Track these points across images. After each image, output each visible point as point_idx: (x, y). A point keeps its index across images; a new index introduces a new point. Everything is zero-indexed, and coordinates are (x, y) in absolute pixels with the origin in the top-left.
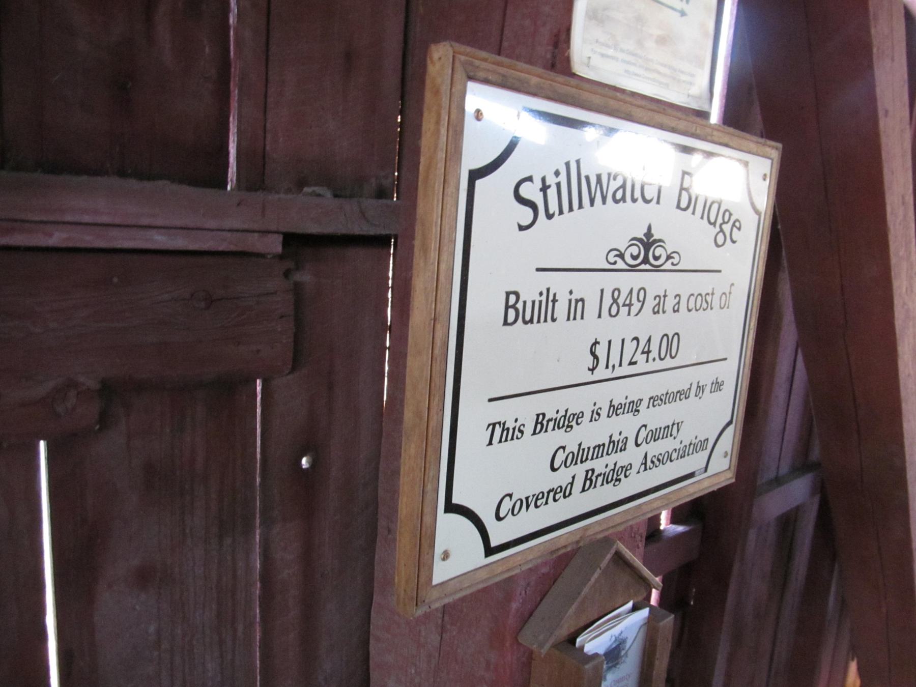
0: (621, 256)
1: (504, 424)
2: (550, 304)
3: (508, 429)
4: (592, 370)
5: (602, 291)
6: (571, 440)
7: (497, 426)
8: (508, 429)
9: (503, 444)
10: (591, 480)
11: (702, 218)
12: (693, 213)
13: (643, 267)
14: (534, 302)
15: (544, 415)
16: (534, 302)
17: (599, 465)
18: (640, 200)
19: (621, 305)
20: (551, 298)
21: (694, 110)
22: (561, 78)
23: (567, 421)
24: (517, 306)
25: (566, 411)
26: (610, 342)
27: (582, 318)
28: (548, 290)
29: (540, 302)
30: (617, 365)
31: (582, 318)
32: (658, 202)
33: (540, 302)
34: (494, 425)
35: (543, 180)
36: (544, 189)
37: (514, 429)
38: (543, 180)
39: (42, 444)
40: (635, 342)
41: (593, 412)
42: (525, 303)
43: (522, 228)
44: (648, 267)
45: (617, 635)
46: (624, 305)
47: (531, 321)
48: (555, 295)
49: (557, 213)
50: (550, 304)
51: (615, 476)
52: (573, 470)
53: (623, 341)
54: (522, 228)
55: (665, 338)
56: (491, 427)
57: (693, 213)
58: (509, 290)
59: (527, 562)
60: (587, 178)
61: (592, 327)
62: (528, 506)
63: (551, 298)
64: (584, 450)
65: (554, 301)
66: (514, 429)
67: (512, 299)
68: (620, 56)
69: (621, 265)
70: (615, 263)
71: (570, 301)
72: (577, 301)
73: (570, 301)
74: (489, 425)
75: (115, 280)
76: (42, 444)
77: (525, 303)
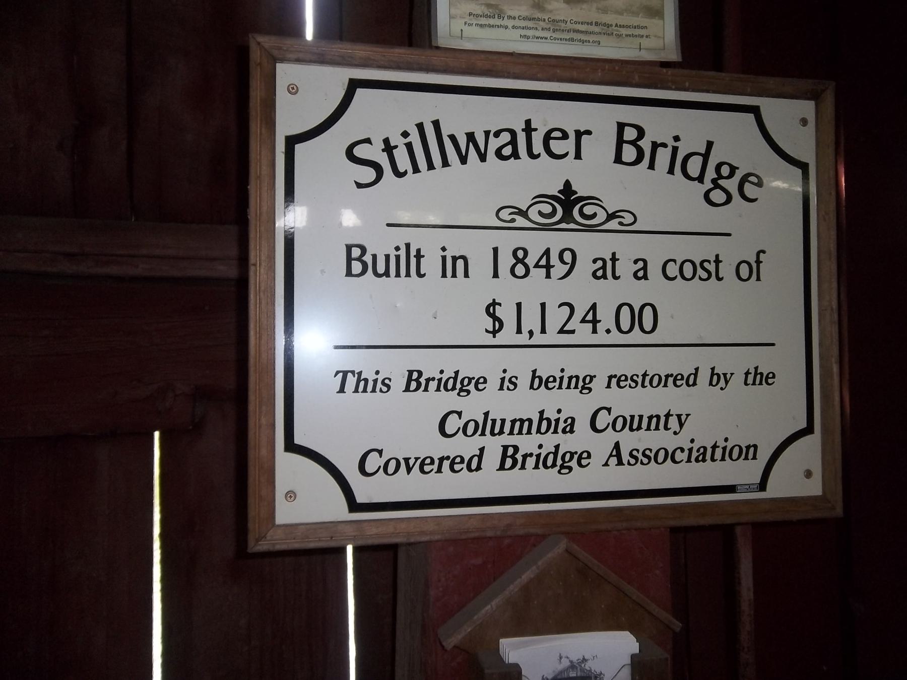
0: (524, 214)
1: (360, 373)
2: (413, 261)
3: (366, 380)
4: (494, 333)
5: (496, 250)
6: (473, 406)
7: (350, 375)
8: (366, 380)
9: (360, 395)
10: (513, 457)
11: (671, 171)
12: (651, 166)
13: (563, 226)
14: (387, 257)
15: (420, 373)
16: (387, 257)
17: (527, 443)
18: (544, 154)
19: (531, 266)
20: (413, 253)
21: (661, 62)
22: (429, 52)
23: (461, 385)
24: (364, 258)
25: (457, 373)
26: (519, 305)
27: (466, 275)
28: (408, 246)
29: (398, 258)
30: (537, 329)
31: (466, 275)
32: (578, 156)
33: (398, 258)
34: (345, 373)
35: (386, 141)
36: (389, 148)
37: (375, 381)
38: (386, 141)
39: (157, 434)
40: (566, 309)
41: (503, 379)
42: (374, 257)
43: (359, 185)
44: (572, 226)
45: (575, 657)
46: (537, 266)
47: (387, 274)
48: (418, 251)
49: (410, 170)
50: (413, 261)
51: (563, 462)
52: (478, 441)
53: (543, 305)
54: (359, 185)
55: (625, 309)
56: (341, 375)
57: (651, 166)
58: (350, 242)
59: (423, 533)
60: (453, 138)
61: (481, 286)
62: (409, 470)
63: (413, 253)
64: (494, 421)
65: (419, 256)
66: (375, 381)
67: (356, 252)
68: (510, 23)
69: (521, 222)
70: (513, 220)
71: (444, 258)
72: (455, 259)
73: (444, 258)
74: (337, 373)
75: (207, 308)
76: (157, 434)
77: (374, 257)
